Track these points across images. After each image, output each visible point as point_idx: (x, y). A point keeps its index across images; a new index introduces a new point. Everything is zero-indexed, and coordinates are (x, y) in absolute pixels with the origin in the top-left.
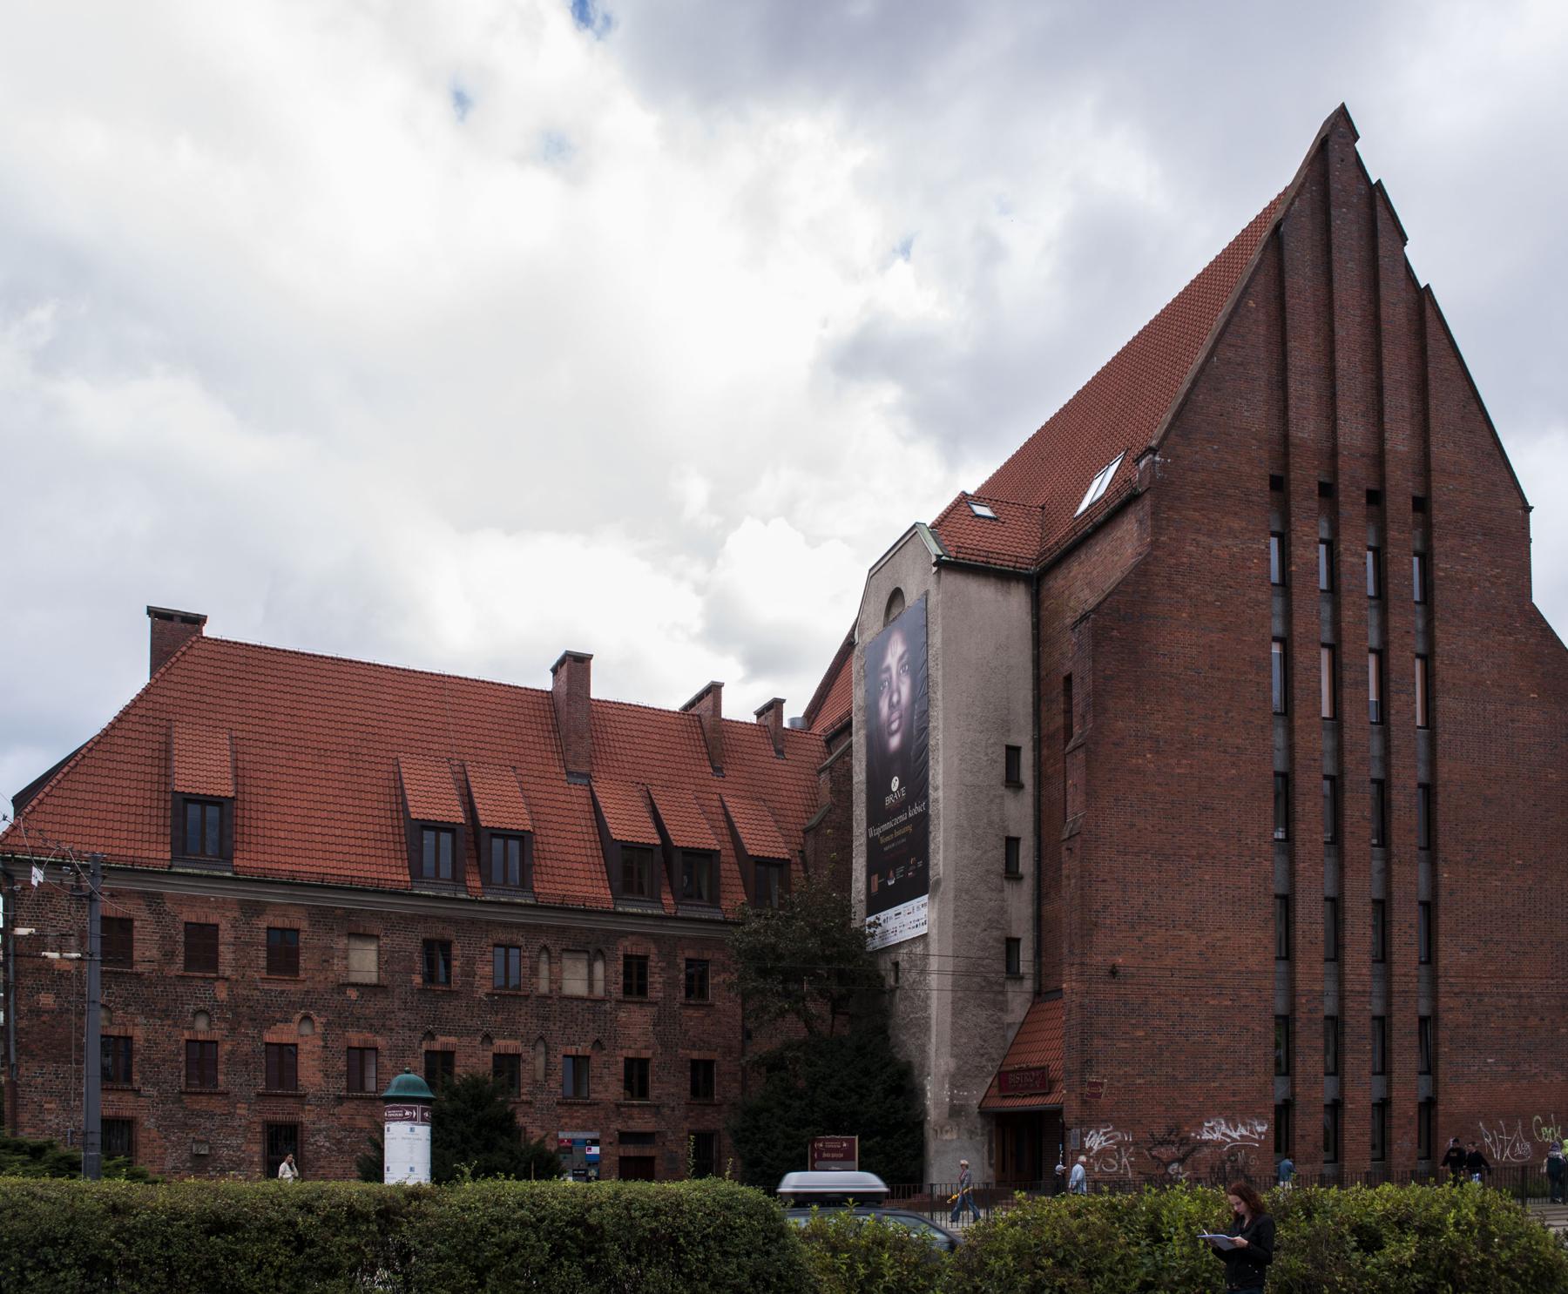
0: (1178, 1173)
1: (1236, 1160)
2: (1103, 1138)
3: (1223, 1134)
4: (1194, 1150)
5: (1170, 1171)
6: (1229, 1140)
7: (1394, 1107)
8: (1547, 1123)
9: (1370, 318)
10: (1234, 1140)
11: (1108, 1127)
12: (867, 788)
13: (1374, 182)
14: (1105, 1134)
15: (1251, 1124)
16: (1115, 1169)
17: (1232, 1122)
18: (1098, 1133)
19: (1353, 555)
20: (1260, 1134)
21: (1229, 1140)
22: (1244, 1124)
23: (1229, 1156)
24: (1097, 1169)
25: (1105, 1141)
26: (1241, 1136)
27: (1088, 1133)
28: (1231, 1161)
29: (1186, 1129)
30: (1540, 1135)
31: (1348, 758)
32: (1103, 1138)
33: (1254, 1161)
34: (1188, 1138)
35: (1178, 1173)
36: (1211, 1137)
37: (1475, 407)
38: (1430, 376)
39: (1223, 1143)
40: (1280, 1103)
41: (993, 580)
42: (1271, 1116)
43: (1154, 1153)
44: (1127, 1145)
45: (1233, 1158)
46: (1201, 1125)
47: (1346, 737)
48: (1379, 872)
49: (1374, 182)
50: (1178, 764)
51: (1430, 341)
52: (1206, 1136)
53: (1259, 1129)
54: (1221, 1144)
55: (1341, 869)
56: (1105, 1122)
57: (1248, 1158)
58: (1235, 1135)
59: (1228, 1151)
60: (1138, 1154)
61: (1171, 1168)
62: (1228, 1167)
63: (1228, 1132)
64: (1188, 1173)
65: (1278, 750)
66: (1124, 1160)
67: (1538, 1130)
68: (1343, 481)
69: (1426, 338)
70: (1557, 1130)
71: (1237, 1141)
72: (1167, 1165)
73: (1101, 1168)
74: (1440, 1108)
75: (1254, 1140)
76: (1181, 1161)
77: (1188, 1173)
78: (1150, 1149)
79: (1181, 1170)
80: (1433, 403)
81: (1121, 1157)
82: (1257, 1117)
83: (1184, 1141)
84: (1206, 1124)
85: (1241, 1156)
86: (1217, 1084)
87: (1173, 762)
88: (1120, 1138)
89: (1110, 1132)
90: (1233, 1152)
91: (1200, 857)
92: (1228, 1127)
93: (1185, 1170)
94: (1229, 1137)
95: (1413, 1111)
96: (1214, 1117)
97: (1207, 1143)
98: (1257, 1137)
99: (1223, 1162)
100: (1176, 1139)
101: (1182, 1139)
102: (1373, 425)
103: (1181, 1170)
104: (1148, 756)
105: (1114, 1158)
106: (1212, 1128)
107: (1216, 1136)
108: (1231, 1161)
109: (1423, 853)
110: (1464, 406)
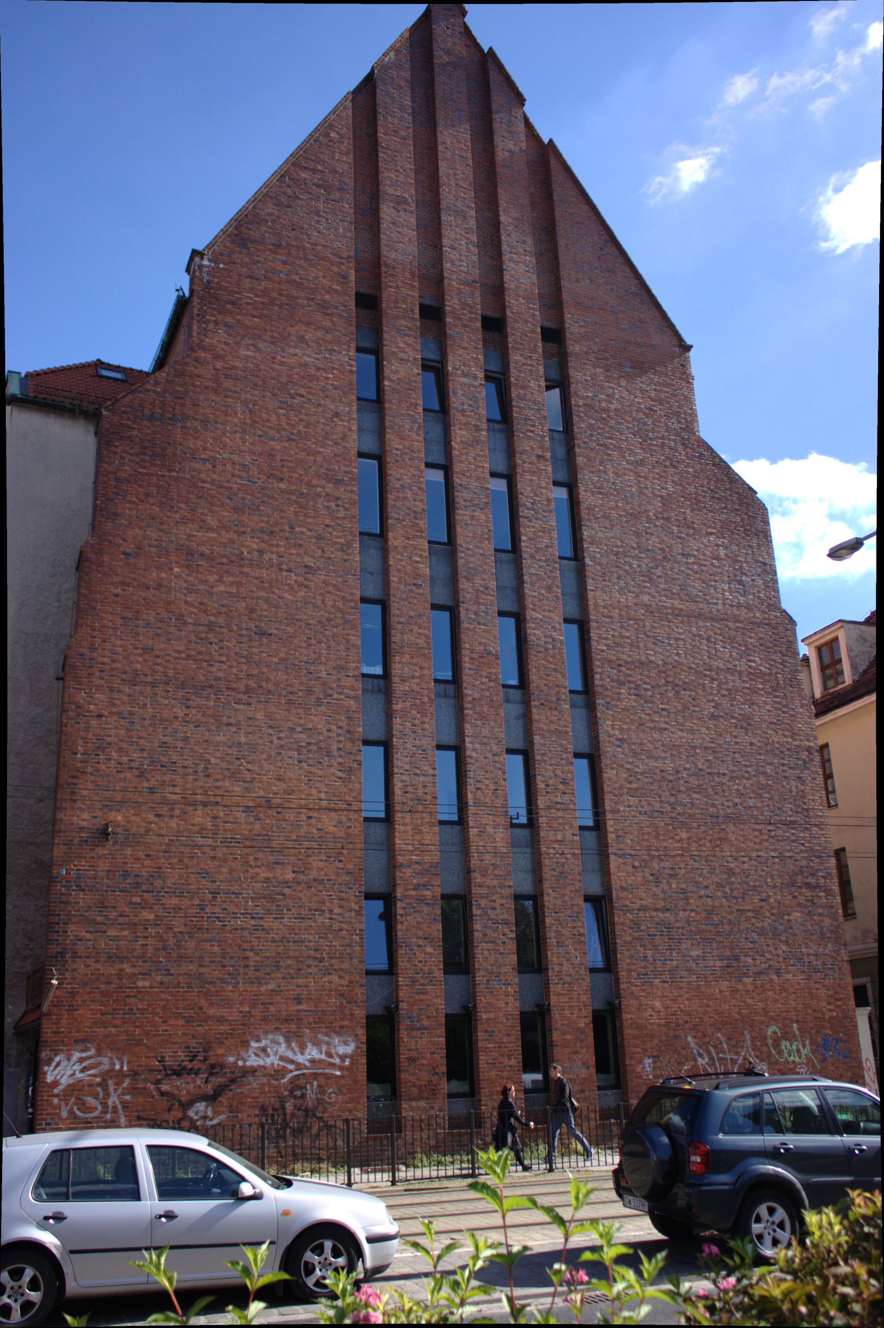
0: (205, 1117)
1: (303, 1096)
2: (77, 1067)
3: (282, 1058)
4: (233, 1081)
5: (191, 1113)
6: (291, 1067)
7: (556, 1015)
8: (787, 1035)
9: (486, 164)
10: (299, 1066)
11: (85, 1050)
12: (368, 1068)
13: (486, 50)
14: (81, 1060)
15: (328, 1044)
16: (96, 1113)
17: (295, 1037)
18: (69, 1059)
19: (464, 375)
20: (343, 1057)
21: (291, 1067)
22: (317, 1043)
23: (291, 1091)
24: (64, 1114)
25: (82, 1071)
26: (313, 1061)
27: (51, 1060)
28: (295, 1097)
29: (220, 1051)
30: (780, 1052)
31: (463, 584)
32: (77, 1067)
33: (331, 1095)
34: (222, 1066)
35: (205, 1117)
36: (262, 1063)
37: (613, 250)
38: (557, 218)
39: (282, 1071)
40: (379, 1011)
41: (82, 422)
42: (361, 1032)
43: (164, 1087)
44: (120, 1076)
45: (299, 1093)
46: (245, 1044)
47: (461, 562)
48: (517, 718)
49: (486, 50)
50: (220, 581)
51: (556, 187)
52: (253, 1061)
53: (341, 1050)
54: (279, 1073)
55: (460, 710)
56: (82, 1042)
57: (323, 1093)
58: (300, 1059)
59: (291, 1081)
60: (133, 1090)
61: (194, 1109)
62: (289, 1107)
63: (290, 1054)
64: (222, 1117)
65: (371, 574)
66: (113, 1100)
67: (777, 1045)
68: (452, 303)
69: (551, 185)
70: (804, 1047)
71: (306, 1068)
72: (191, 1103)
73: (71, 1113)
74: (625, 1016)
75: (332, 1065)
76: (211, 1099)
77: (222, 1117)
78: (158, 1082)
79: (210, 1113)
80: (562, 243)
81: (107, 1095)
82: (337, 1033)
83: (215, 1069)
84: (254, 1044)
85: (311, 1092)
86: (271, 986)
87: (212, 579)
88: (105, 1067)
89: (90, 1057)
90: (296, 1085)
91: (248, 691)
92: (289, 1046)
93: (217, 1113)
94: (292, 1062)
95: (584, 1022)
96: (266, 1033)
97: (253, 1071)
98: (337, 1061)
99: (282, 1100)
100: (203, 1067)
101: (213, 1067)
102: (492, 258)
103: (210, 1113)
104: (176, 570)
105: (96, 1096)
106: (264, 1050)
107: (272, 1061)
108: (295, 1097)
109: (579, 698)
110: (601, 249)
